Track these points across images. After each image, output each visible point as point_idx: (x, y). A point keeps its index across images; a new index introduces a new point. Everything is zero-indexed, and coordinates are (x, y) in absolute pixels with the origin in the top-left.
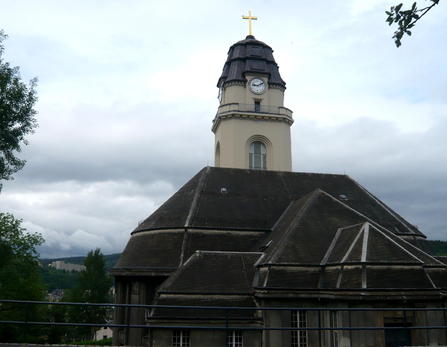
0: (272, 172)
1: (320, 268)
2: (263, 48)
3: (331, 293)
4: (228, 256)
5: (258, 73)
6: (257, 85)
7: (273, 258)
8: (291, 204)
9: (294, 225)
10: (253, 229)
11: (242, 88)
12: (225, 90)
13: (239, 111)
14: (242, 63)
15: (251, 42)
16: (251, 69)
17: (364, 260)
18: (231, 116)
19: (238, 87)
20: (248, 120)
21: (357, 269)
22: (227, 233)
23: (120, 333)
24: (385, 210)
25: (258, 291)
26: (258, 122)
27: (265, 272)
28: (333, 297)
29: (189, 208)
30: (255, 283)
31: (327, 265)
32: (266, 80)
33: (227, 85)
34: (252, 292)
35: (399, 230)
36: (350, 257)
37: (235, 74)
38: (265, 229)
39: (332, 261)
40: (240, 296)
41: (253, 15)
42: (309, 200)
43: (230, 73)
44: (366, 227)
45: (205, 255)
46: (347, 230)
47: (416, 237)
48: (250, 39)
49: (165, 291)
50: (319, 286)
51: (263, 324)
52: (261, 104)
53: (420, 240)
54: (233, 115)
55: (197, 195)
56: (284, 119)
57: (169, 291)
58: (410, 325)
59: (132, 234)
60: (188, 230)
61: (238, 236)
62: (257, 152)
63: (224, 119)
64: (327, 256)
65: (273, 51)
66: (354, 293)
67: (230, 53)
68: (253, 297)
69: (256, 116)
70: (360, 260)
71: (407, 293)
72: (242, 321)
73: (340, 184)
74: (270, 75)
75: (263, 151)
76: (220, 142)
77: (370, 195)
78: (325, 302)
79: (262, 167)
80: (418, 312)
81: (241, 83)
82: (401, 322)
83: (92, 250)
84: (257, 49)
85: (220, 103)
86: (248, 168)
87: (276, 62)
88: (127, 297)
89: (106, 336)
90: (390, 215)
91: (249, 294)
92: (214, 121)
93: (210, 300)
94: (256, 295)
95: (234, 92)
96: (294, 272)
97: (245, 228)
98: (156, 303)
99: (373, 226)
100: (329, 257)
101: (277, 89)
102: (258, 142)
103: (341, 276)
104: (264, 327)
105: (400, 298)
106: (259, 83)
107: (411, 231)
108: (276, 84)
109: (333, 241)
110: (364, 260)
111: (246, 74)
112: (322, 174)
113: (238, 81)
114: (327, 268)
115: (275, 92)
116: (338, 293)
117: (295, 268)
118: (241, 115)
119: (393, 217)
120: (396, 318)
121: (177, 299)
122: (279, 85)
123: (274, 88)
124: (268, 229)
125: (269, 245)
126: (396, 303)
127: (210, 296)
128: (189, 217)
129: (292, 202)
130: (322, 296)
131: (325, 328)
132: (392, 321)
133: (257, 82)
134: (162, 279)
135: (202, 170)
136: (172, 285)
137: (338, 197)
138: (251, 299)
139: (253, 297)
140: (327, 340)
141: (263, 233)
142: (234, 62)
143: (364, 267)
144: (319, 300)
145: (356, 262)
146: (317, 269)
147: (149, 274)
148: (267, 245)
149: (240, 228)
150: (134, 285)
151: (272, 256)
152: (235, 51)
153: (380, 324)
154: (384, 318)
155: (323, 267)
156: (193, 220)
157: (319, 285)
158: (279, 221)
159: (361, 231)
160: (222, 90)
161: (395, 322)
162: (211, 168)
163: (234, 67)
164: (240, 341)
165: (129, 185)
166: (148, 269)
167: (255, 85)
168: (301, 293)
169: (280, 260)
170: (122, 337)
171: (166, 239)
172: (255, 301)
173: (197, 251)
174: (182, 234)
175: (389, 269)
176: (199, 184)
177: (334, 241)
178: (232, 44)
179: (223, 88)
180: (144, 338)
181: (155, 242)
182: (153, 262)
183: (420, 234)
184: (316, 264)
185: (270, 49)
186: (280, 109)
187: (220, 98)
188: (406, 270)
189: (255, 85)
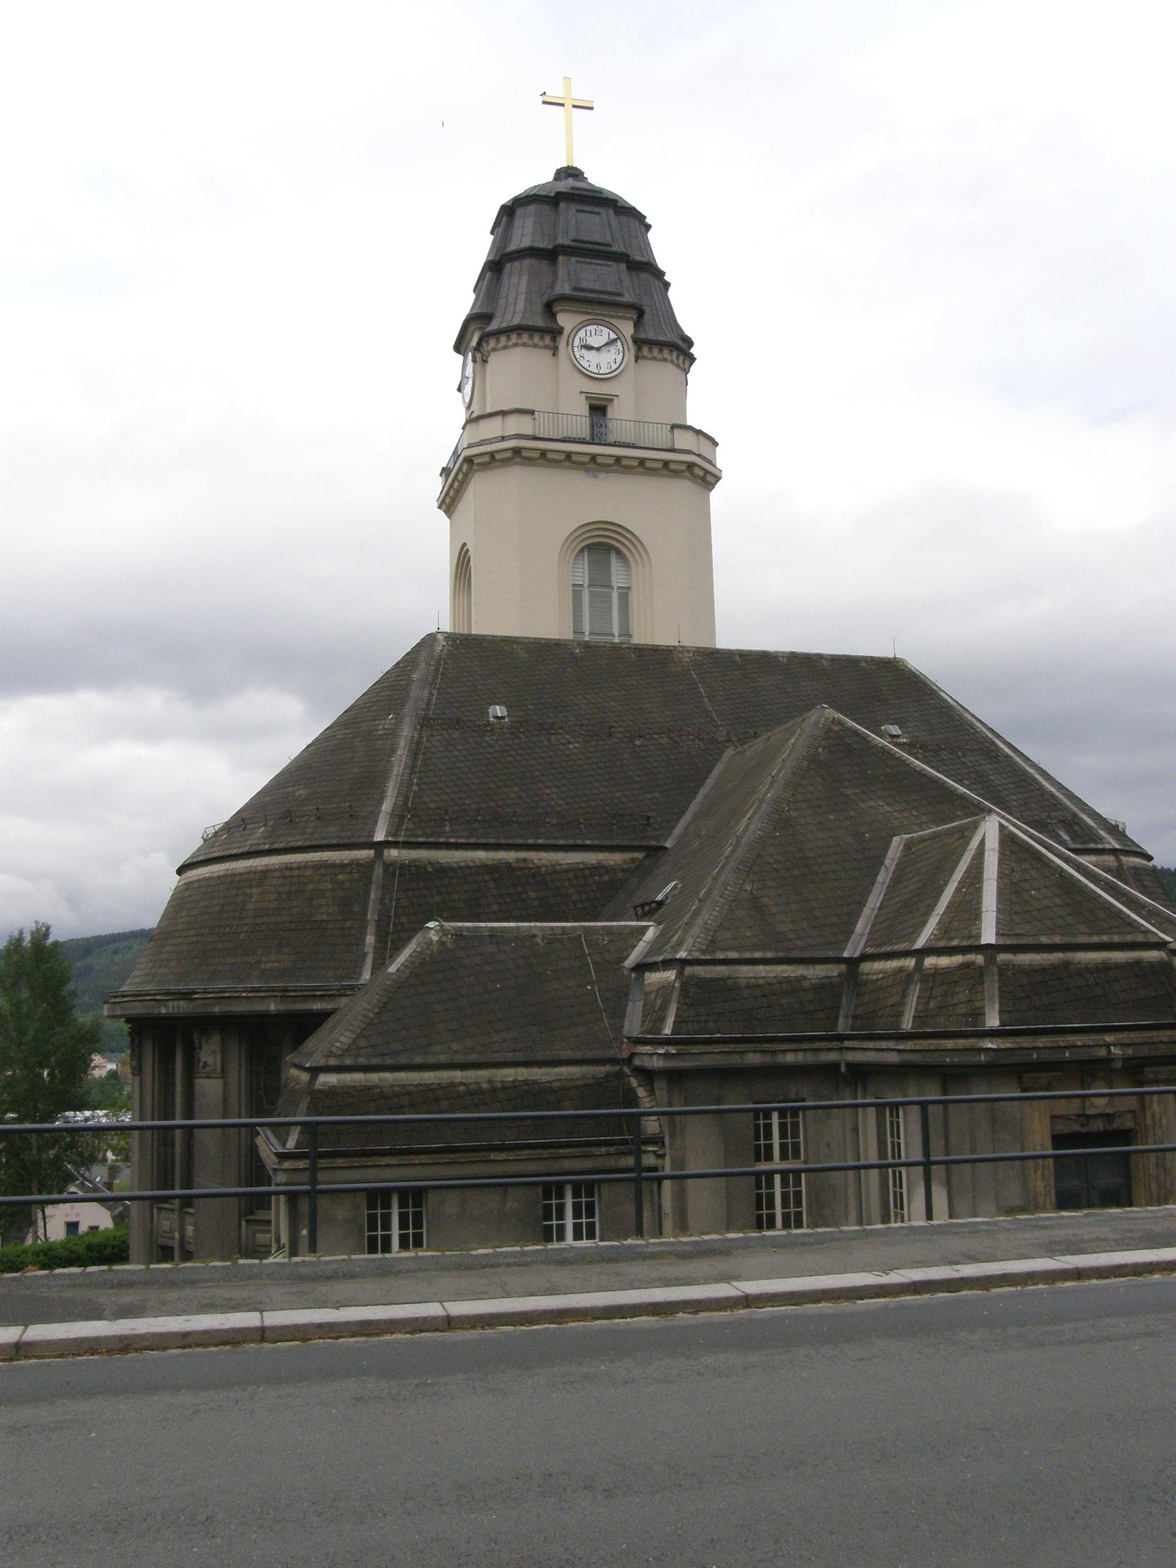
0: (656, 650)
1: (843, 967)
2: (616, 213)
3: (883, 1044)
4: (534, 936)
5: (599, 305)
6: (598, 348)
7: (690, 941)
8: (725, 757)
9: (750, 825)
10: (607, 843)
11: (543, 356)
12: (485, 361)
13: (535, 438)
14: (544, 265)
15: (570, 194)
16: (575, 289)
17: (989, 936)
18: (509, 454)
19: (519, 351)
20: (616, 472)
21: (966, 966)
22: (518, 860)
23: (159, 1209)
24: (1025, 773)
25: (647, 1049)
26: (602, 475)
27: (664, 990)
28: (892, 1058)
29: (385, 775)
30: (633, 1024)
31: (864, 958)
32: (628, 329)
33: (492, 343)
34: (625, 1055)
35: (1073, 839)
36: (945, 928)
37: (521, 305)
38: (645, 843)
39: (882, 944)
40: (584, 1069)
41: (580, 94)
42: (795, 741)
43: (502, 302)
44: (990, 829)
45: (459, 935)
46: (922, 840)
47: (1124, 859)
48: (570, 182)
49: (332, 1062)
50: (842, 1026)
51: (662, 1156)
52: (609, 414)
53: (1136, 870)
54: (517, 451)
55: (407, 732)
56: (691, 466)
57: (348, 1061)
58: (1126, 1136)
59: (180, 871)
60: (386, 852)
61: (554, 871)
62: (600, 580)
63: (485, 466)
64: (862, 926)
65: (648, 227)
66: (962, 1043)
67: (500, 230)
68: (626, 1070)
69: (593, 458)
70: (978, 936)
71: (1123, 1036)
72: (594, 1150)
73: (881, 685)
74: (641, 313)
75: (618, 576)
76: (469, 546)
77: (978, 724)
78: (860, 1075)
79: (616, 631)
80: (1155, 1097)
81: (542, 338)
82: (1102, 1128)
83: (21, 933)
84: (596, 218)
85: (469, 407)
86: (568, 635)
87: (661, 265)
88: (179, 1088)
89: (97, 1228)
90: (1041, 787)
91: (614, 1061)
92: (445, 471)
93: (485, 1086)
94: (637, 1062)
95: (517, 370)
96: (761, 982)
97: (579, 842)
98: (304, 1104)
99: (1012, 828)
100: (871, 933)
101: (665, 360)
102: (602, 547)
103: (915, 992)
104: (668, 1171)
105: (1102, 1053)
106: (604, 340)
107: (1109, 838)
108: (661, 345)
109: (880, 878)
110: (989, 936)
111: (557, 307)
112: (820, 656)
113: (531, 330)
114: (866, 967)
115: (659, 372)
116: (909, 1045)
117: (761, 970)
118: (543, 453)
119: (1053, 795)
120: (1088, 1117)
121: (376, 1087)
122: (672, 346)
123: (654, 359)
124: (653, 843)
125: (666, 897)
126: (1089, 1069)
127: (484, 1073)
128: (387, 806)
129: (729, 752)
130: (851, 1057)
131: (862, 1162)
132: (1076, 1128)
133: (598, 335)
134: (305, 1025)
135: (419, 645)
136: (354, 1041)
137: (878, 734)
138: (620, 1075)
139: (626, 1070)
140: (868, 1198)
141: (639, 855)
142: (517, 264)
143: (991, 960)
144: (843, 1069)
145: (965, 943)
146: (834, 970)
147: (258, 1007)
148: (659, 898)
149: (561, 842)
150: (204, 1045)
151: (686, 932)
152: (517, 222)
153: (1039, 1139)
154: (1053, 1117)
155: (853, 963)
156: (402, 818)
157: (841, 1020)
158: (688, 817)
159: (974, 844)
160: (474, 361)
161: (1084, 1130)
162: (450, 637)
163: (515, 279)
164: (590, 1214)
165: (153, 702)
166: (254, 990)
167: (589, 348)
168: (784, 1051)
169: (713, 944)
170: (166, 1225)
171: (311, 887)
172: (634, 1082)
173: (431, 925)
174: (365, 868)
175: (1066, 964)
176: (413, 693)
177: (884, 877)
178: (506, 197)
179: (478, 356)
180: (247, 1221)
181: (273, 897)
182: (269, 965)
183: (1135, 849)
184: (831, 954)
185: (640, 218)
186: (676, 431)
187: (468, 389)
188: (1119, 966)
189: (589, 348)
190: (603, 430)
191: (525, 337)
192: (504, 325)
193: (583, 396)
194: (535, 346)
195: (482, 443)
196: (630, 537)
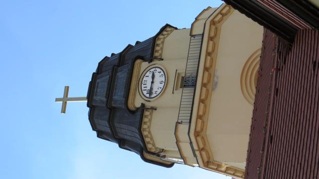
6: (152, 81)
54: (197, 134)
56: (213, 23)
111: (133, 109)
123: (162, 49)
179: (162, 154)
190: (190, 79)
191: (144, 126)
192: (139, 137)
193: (175, 91)
194: (150, 120)
195: (195, 155)
196: (249, 63)
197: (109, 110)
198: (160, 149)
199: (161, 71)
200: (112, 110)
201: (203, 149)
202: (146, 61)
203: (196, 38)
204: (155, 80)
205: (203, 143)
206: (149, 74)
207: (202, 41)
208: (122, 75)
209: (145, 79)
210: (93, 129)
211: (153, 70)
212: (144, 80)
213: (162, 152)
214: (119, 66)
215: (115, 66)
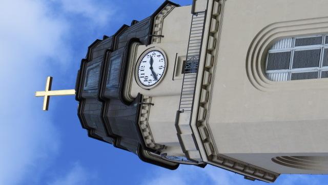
197: (101, 103)
198: (161, 146)
199: (160, 54)
200: (104, 100)
201: (206, 140)
202: (143, 44)
203: (198, 16)
204: (150, 72)
205: (206, 134)
206: (147, 59)
207: (195, 88)
208: (116, 64)
209: (142, 64)
210: (83, 127)
211: (151, 54)
212: (141, 66)
213: (163, 148)
214: (112, 51)
215: (108, 50)
